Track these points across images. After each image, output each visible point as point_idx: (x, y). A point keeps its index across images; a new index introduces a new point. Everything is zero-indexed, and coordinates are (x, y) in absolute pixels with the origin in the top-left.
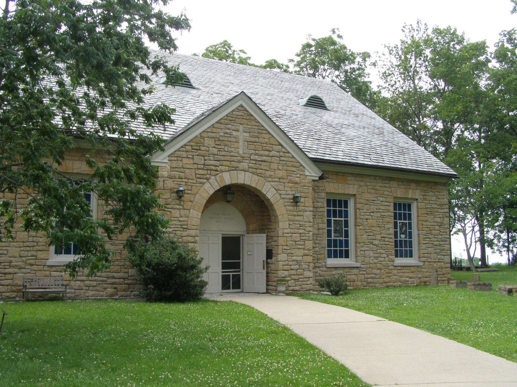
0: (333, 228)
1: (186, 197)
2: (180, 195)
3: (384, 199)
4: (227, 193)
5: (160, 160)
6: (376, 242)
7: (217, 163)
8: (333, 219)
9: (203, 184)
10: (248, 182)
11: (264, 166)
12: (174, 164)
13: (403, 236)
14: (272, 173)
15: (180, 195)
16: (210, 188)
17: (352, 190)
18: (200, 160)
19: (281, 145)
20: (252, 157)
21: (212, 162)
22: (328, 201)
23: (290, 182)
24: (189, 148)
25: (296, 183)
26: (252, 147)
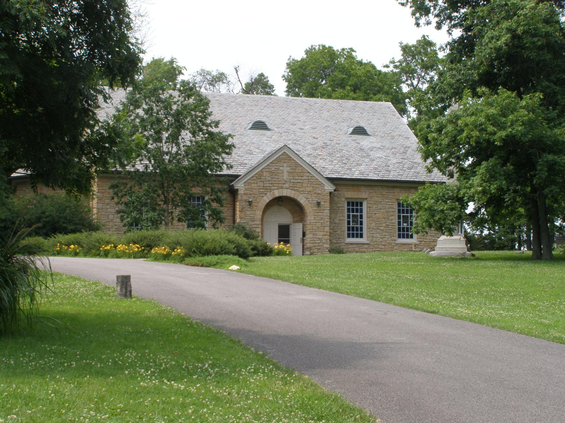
0: (351, 220)
1: (254, 204)
2: (250, 203)
3: (389, 201)
4: (279, 201)
5: (239, 185)
6: (382, 228)
7: (271, 185)
8: (402, 215)
9: (263, 197)
10: (289, 195)
11: (298, 185)
12: (247, 187)
13: (405, 224)
14: (304, 189)
15: (250, 203)
16: (267, 199)
17: (364, 195)
18: (261, 184)
19: (309, 172)
20: (292, 181)
21: (268, 185)
22: (348, 204)
23: (315, 193)
24: (254, 178)
25: (319, 194)
26: (292, 175)
